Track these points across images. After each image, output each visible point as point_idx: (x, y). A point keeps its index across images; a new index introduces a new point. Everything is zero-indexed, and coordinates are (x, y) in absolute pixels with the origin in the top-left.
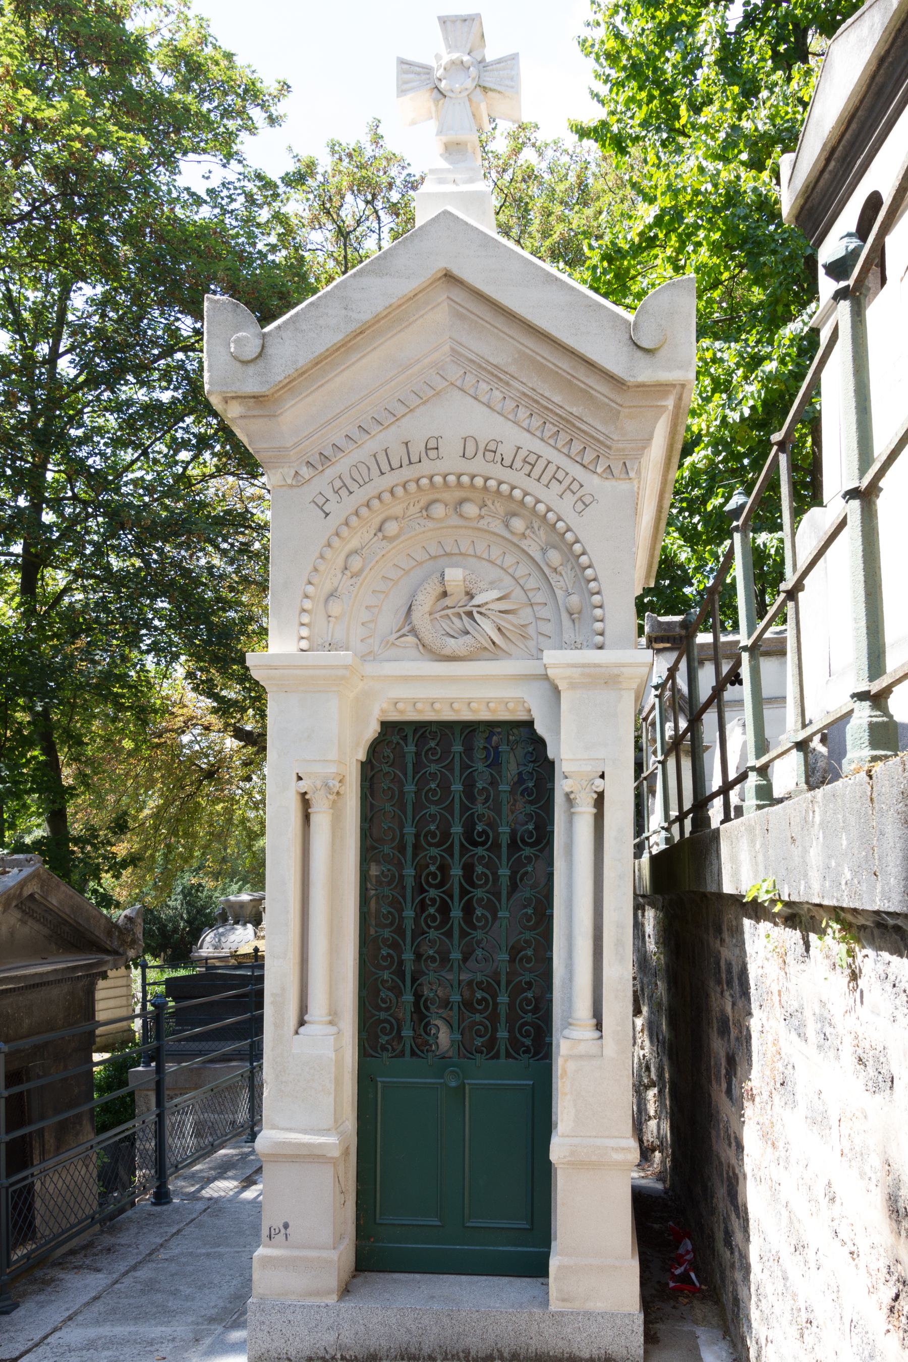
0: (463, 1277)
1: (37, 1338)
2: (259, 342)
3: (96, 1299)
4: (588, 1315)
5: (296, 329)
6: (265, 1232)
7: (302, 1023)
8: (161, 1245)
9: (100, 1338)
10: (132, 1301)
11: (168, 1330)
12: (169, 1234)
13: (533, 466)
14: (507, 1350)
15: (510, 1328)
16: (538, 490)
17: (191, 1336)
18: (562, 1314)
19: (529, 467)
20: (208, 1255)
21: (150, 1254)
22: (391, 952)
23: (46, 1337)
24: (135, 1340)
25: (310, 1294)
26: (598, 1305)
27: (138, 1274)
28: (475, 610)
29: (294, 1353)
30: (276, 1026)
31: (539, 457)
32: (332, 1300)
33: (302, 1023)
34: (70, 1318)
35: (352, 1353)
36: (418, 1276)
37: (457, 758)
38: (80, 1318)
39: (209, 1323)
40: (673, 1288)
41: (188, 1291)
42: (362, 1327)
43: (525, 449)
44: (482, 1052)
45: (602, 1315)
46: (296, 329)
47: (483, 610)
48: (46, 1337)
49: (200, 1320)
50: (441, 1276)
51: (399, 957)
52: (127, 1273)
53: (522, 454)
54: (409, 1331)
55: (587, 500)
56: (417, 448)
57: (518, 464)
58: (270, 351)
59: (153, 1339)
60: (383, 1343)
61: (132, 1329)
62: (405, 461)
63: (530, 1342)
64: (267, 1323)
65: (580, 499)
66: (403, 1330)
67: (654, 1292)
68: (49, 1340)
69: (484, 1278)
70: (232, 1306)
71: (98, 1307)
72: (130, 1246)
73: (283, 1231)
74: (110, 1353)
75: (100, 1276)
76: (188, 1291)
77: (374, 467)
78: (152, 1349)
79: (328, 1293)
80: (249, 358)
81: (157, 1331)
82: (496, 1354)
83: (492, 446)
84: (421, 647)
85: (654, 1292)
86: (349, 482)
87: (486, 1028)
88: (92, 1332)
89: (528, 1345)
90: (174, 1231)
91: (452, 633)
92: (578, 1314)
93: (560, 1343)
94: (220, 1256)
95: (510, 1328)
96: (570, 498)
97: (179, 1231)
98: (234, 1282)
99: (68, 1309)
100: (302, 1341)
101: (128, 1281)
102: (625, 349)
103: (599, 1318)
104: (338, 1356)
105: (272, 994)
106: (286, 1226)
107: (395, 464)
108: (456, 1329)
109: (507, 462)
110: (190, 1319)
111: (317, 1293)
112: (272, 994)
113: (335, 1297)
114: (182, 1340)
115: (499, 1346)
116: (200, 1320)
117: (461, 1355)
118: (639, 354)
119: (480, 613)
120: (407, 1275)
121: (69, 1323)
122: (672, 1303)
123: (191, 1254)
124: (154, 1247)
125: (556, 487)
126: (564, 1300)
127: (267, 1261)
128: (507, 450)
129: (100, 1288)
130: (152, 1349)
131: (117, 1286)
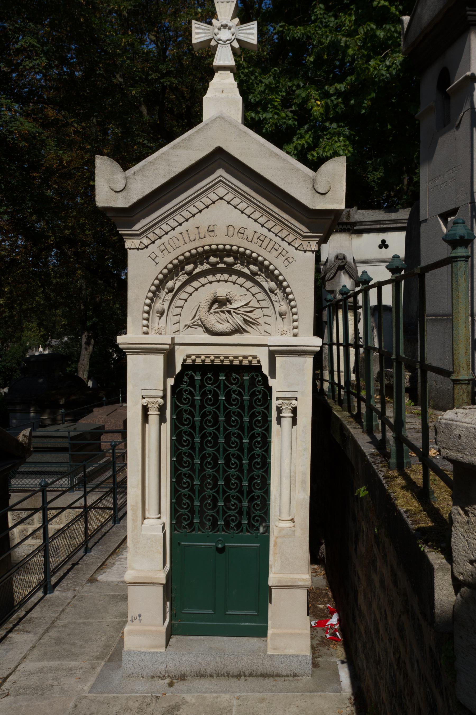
0: (225, 638)
1: (13, 667)
2: (123, 182)
3: (33, 647)
4: (286, 656)
5: (143, 175)
6: (129, 619)
7: (144, 518)
8: (57, 618)
9: (44, 667)
10: (53, 648)
11: (77, 663)
12: (59, 612)
13: (263, 241)
14: (247, 672)
15: (249, 662)
16: (264, 253)
17: (89, 666)
18: (273, 655)
19: (260, 242)
20: (84, 623)
21: (53, 623)
22: (188, 480)
23: (16, 667)
24: (62, 668)
25: (153, 647)
26: (291, 652)
27: (50, 634)
28: (232, 310)
29: (145, 674)
30: (133, 520)
31: (266, 237)
32: (163, 650)
33: (144, 518)
34: (24, 658)
35: (173, 674)
36: (202, 637)
37: (222, 383)
38: (29, 657)
39: (97, 660)
40: (329, 638)
41: (81, 643)
42: (178, 662)
43: (259, 233)
44: (234, 530)
45: (293, 656)
46: (143, 175)
47: (236, 311)
48: (16, 667)
49: (92, 658)
50: (214, 637)
51: (192, 483)
52: (44, 634)
53: (257, 235)
54: (200, 664)
55: (290, 260)
56: (204, 230)
57: (255, 240)
58: (129, 186)
59: (71, 668)
60: (188, 669)
61: (58, 663)
62: (197, 237)
63: (258, 668)
64: (132, 661)
65: (286, 259)
66: (197, 664)
67: (318, 642)
68: (18, 669)
69: (235, 638)
70: (105, 651)
71: (36, 652)
72: (40, 618)
73: (138, 618)
74: (52, 675)
75: (30, 635)
76: (81, 643)
77: (181, 240)
78: (73, 672)
79: (160, 647)
80: (119, 190)
81: (72, 664)
82: (242, 674)
83: (242, 231)
84: (286, 678)
85: (318, 642)
86: (168, 247)
87: (236, 517)
88: (40, 665)
89: (257, 669)
90: (61, 610)
91: (220, 321)
92: (281, 655)
93: (273, 669)
94: (91, 624)
95: (249, 662)
96: (281, 259)
97: (63, 610)
98: (103, 639)
99: (21, 653)
100: (149, 668)
101: (46, 638)
102: (310, 192)
103: (291, 657)
104: (167, 675)
105: (131, 505)
106: (140, 616)
107: (192, 238)
108: (223, 663)
109: (250, 240)
110: (87, 658)
111: (156, 647)
112: (131, 505)
113: (164, 648)
114: (86, 668)
115: (243, 670)
116: (92, 658)
117: (225, 674)
118: (318, 195)
119: (234, 312)
120: (197, 637)
121: (25, 660)
122: (327, 647)
123: (75, 623)
124: (53, 619)
125: (275, 253)
126: (274, 649)
127: (130, 633)
128: (249, 233)
129: (33, 642)
130: (73, 672)
131: (41, 641)
